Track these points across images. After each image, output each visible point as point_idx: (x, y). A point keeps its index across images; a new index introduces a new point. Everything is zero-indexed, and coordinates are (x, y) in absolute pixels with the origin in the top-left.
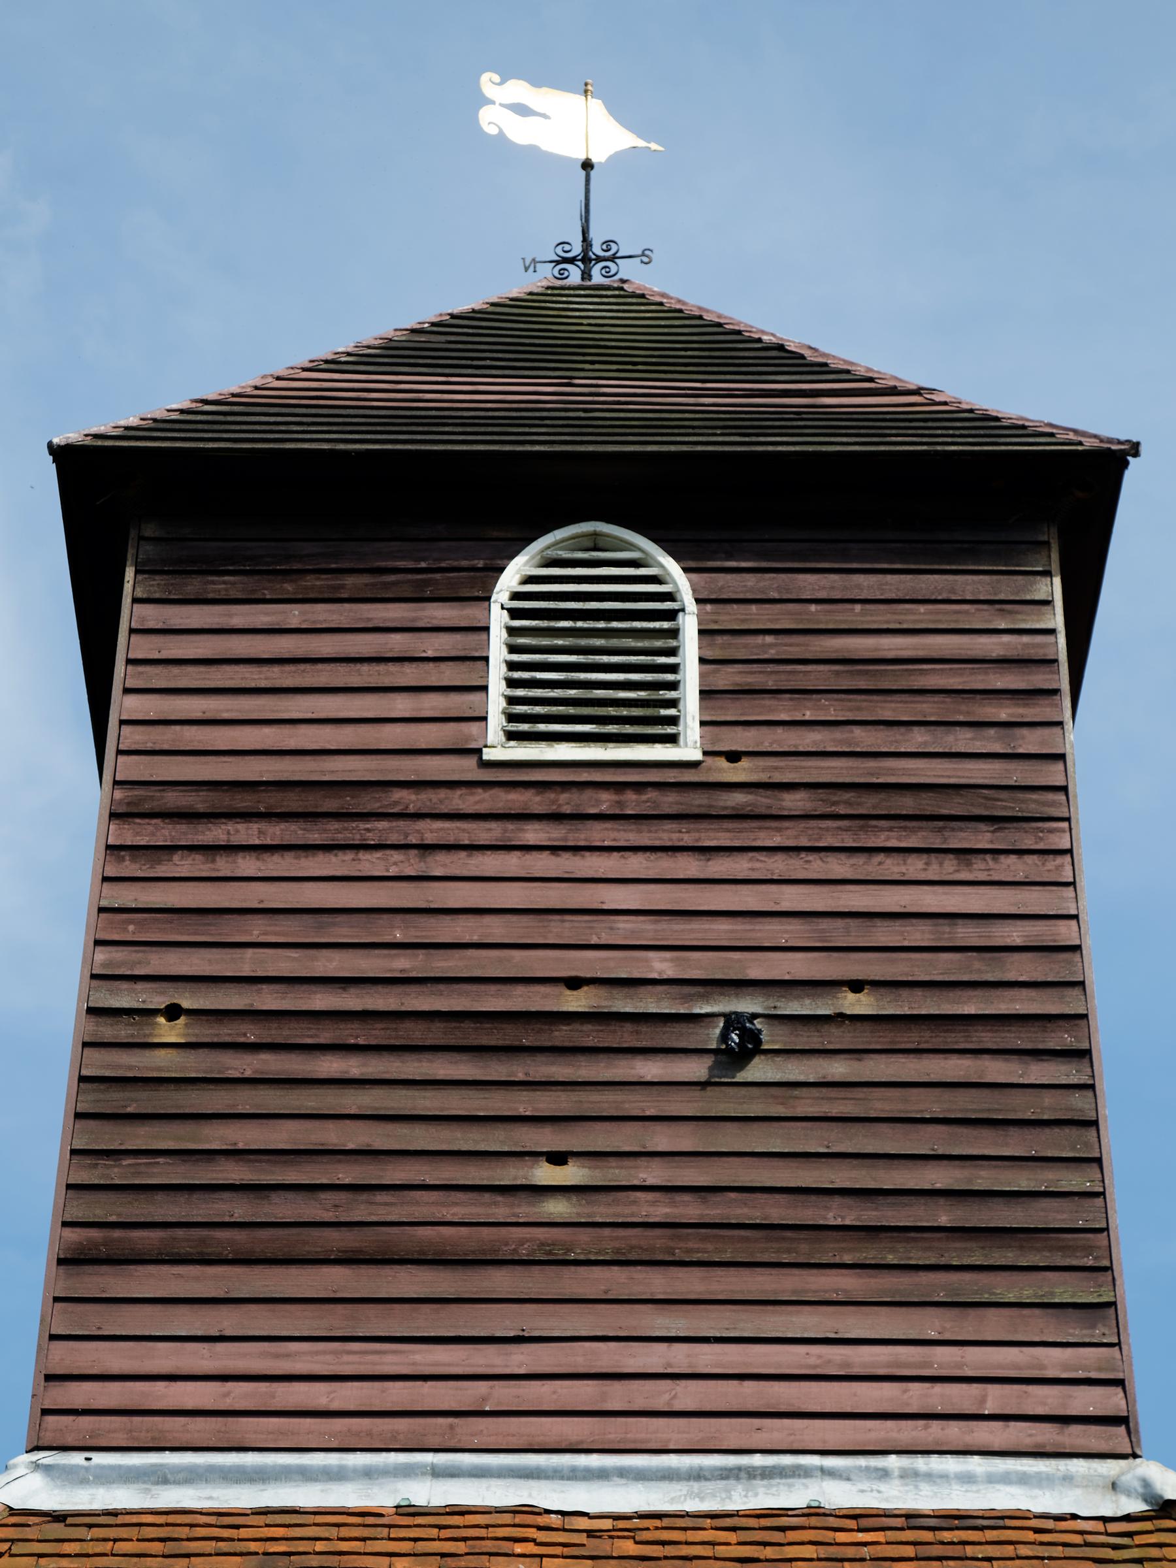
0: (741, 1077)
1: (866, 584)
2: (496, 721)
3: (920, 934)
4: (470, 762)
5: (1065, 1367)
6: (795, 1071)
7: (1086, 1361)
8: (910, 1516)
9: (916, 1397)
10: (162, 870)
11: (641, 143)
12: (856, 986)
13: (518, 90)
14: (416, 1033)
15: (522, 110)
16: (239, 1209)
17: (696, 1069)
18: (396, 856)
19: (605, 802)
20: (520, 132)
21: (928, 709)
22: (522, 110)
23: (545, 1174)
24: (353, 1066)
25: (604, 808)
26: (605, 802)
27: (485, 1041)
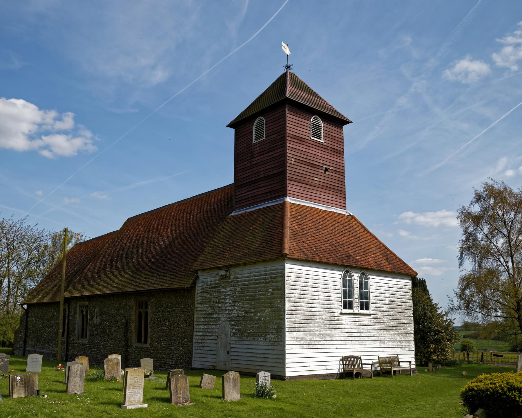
3: (335, 163)
4: (309, 138)
7: (343, 201)
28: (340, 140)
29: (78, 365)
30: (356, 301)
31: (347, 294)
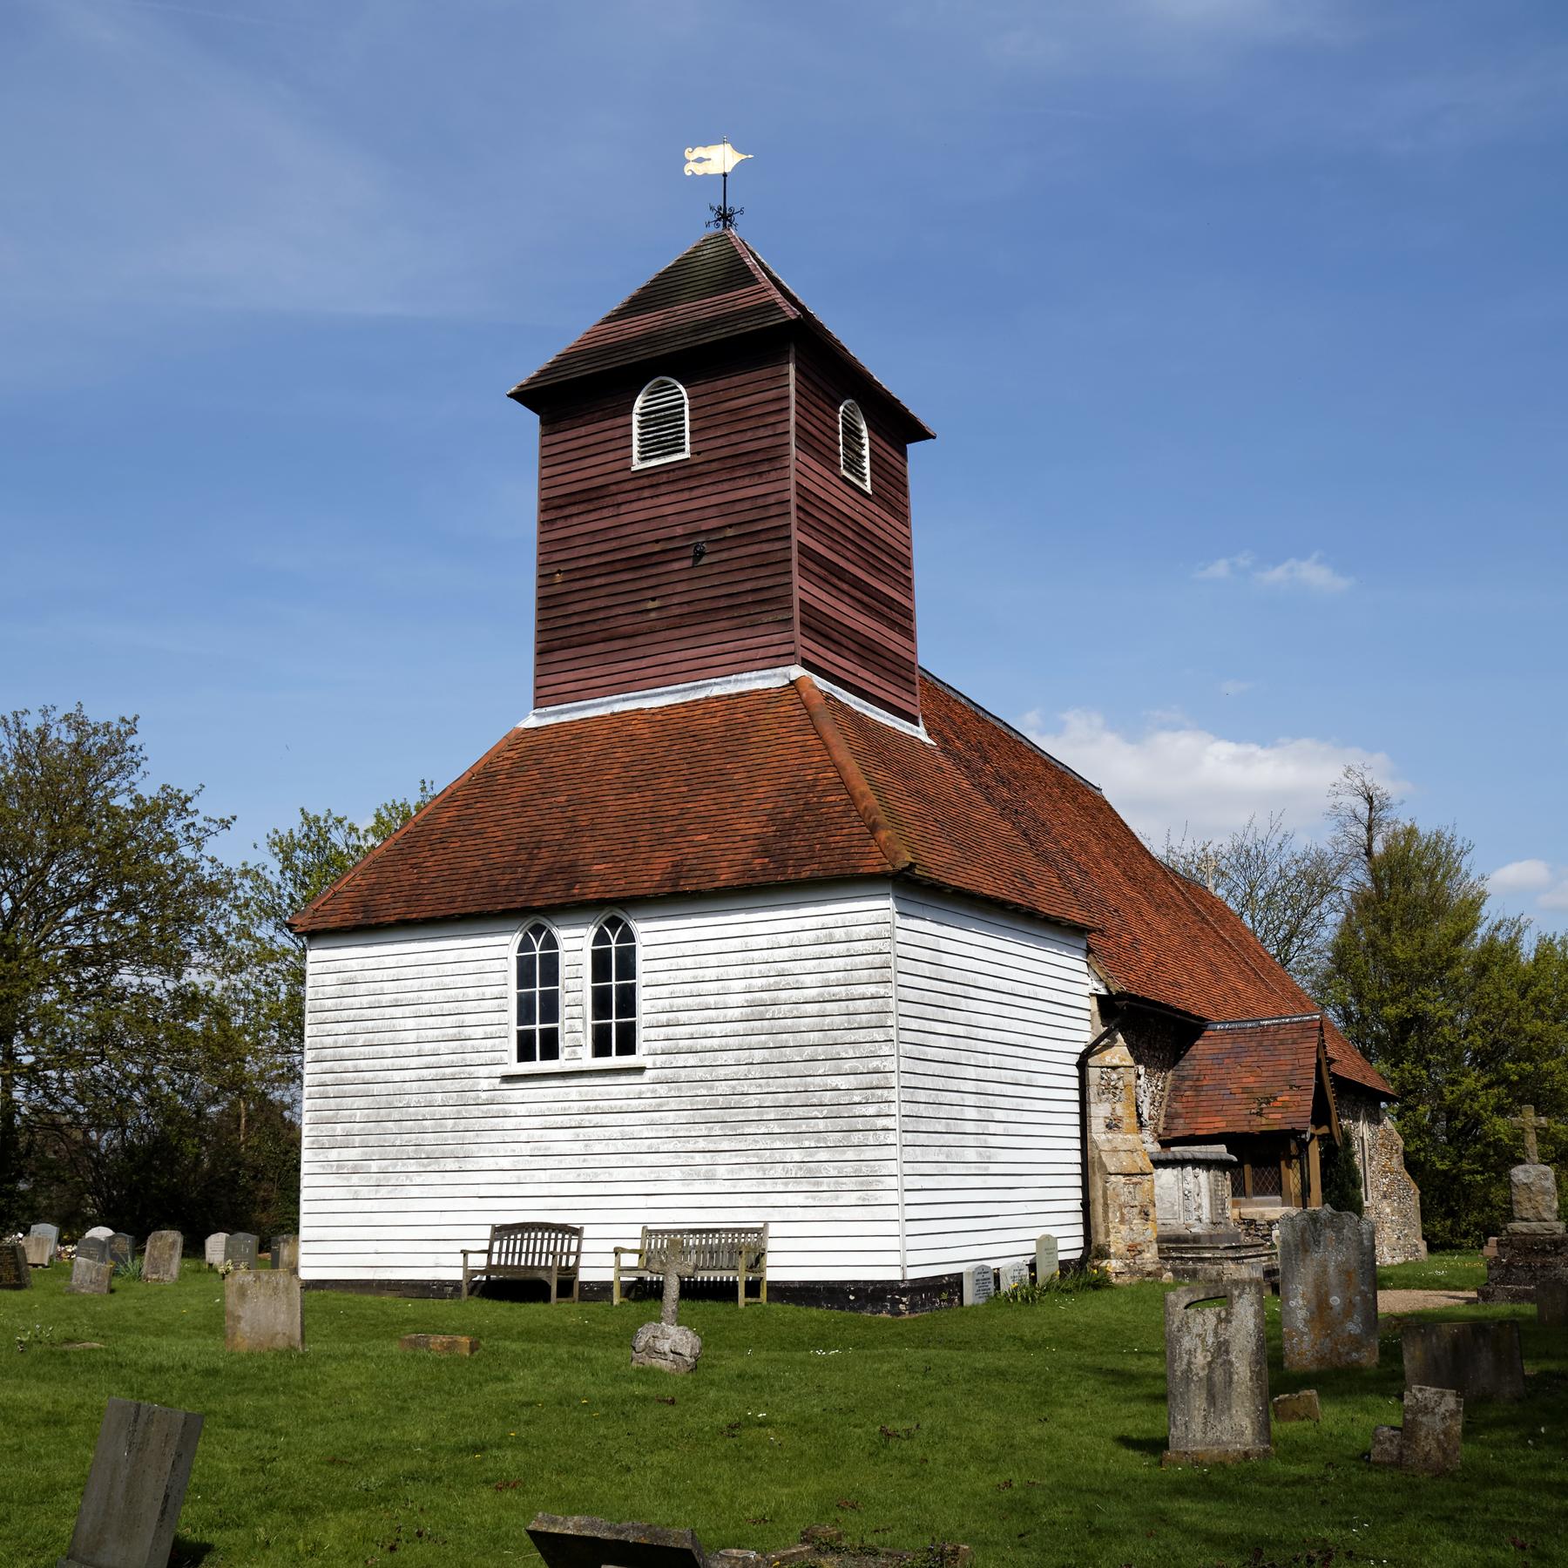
0: (700, 563)
1: (736, 380)
2: (636, 455)
5: (780, 639)
6: (714, 558)
8: (730, 695)
9: (741, 656)
10: (555, 527)
11: (744, 157)
12: (730, 526)
13: (700, 152)
14: (619, 566)
15: (700, 160)
16: (577, 630)
17: (688, 563)
18: (611, 509)
19: (664, 478)
20: (700, 169)
21: (752, 423)
22: (700, 160)
23: (651, 605)
24: (602, 581)
25: (664, 480)
26: (664, 478)
27: (635, 565)
28: (902, 570)
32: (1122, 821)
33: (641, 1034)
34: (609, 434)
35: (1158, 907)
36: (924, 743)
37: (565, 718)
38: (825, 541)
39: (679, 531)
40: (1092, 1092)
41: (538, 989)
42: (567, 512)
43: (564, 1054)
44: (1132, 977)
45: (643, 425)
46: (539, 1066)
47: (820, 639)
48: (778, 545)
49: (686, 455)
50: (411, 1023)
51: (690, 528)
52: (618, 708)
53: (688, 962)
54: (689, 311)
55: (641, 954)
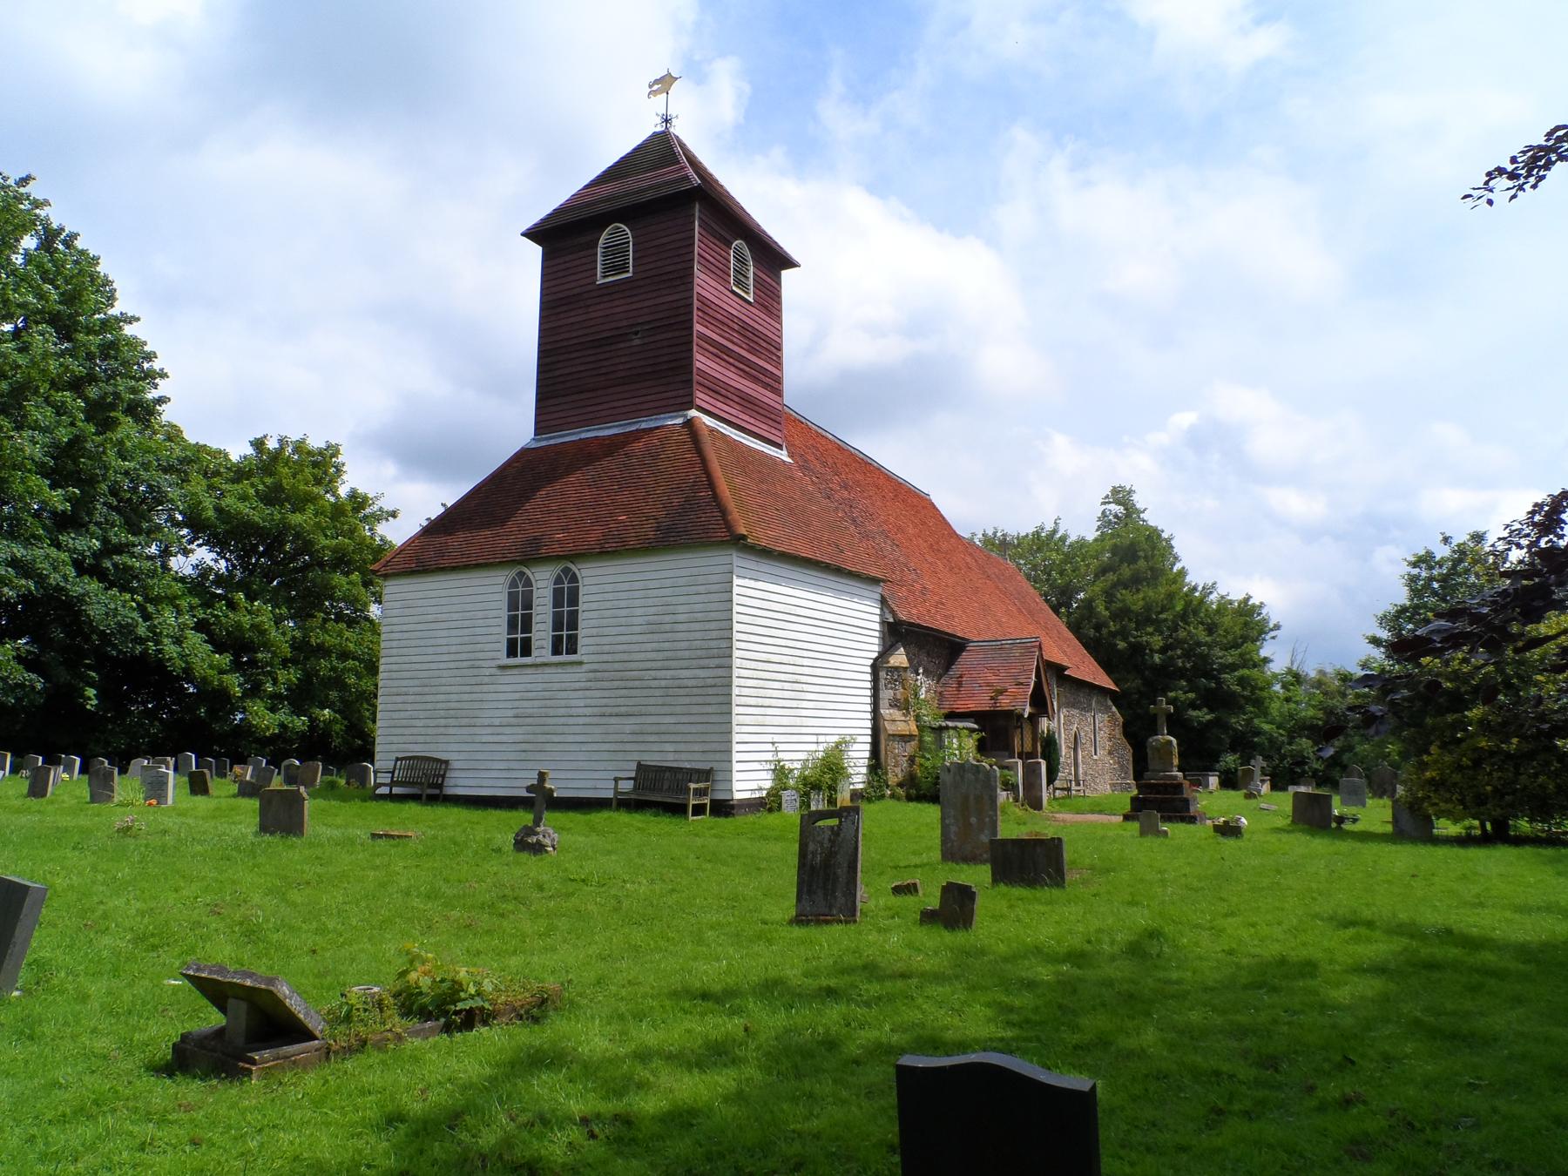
28: (774, 351)
29: (832, 801)
30: (542, 634)
31: (520, 621)
32: (941, 516)
33: (581, 642)
34: (584, 260)
35: (951, 569)
36: (784, 461)
37: (552, 442)
38: (718, 331)
39: (625, 323)
40: (882, 682)
41: (565, 609)
42: (558, 310)
43: (535, 653)
44: (914, 611)
45: (605, 255)
46: (519, 660)
47: (711, 393)
48: (684, 333)
49: (630, 275)
50: (444, 633)
51: (631, 322)
52: (583, 436)
53: (610, 596)
54: (642, 181)
55: (582, 591)
